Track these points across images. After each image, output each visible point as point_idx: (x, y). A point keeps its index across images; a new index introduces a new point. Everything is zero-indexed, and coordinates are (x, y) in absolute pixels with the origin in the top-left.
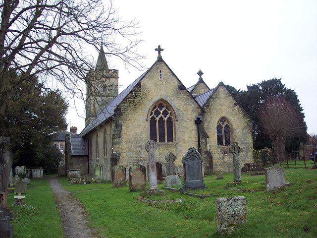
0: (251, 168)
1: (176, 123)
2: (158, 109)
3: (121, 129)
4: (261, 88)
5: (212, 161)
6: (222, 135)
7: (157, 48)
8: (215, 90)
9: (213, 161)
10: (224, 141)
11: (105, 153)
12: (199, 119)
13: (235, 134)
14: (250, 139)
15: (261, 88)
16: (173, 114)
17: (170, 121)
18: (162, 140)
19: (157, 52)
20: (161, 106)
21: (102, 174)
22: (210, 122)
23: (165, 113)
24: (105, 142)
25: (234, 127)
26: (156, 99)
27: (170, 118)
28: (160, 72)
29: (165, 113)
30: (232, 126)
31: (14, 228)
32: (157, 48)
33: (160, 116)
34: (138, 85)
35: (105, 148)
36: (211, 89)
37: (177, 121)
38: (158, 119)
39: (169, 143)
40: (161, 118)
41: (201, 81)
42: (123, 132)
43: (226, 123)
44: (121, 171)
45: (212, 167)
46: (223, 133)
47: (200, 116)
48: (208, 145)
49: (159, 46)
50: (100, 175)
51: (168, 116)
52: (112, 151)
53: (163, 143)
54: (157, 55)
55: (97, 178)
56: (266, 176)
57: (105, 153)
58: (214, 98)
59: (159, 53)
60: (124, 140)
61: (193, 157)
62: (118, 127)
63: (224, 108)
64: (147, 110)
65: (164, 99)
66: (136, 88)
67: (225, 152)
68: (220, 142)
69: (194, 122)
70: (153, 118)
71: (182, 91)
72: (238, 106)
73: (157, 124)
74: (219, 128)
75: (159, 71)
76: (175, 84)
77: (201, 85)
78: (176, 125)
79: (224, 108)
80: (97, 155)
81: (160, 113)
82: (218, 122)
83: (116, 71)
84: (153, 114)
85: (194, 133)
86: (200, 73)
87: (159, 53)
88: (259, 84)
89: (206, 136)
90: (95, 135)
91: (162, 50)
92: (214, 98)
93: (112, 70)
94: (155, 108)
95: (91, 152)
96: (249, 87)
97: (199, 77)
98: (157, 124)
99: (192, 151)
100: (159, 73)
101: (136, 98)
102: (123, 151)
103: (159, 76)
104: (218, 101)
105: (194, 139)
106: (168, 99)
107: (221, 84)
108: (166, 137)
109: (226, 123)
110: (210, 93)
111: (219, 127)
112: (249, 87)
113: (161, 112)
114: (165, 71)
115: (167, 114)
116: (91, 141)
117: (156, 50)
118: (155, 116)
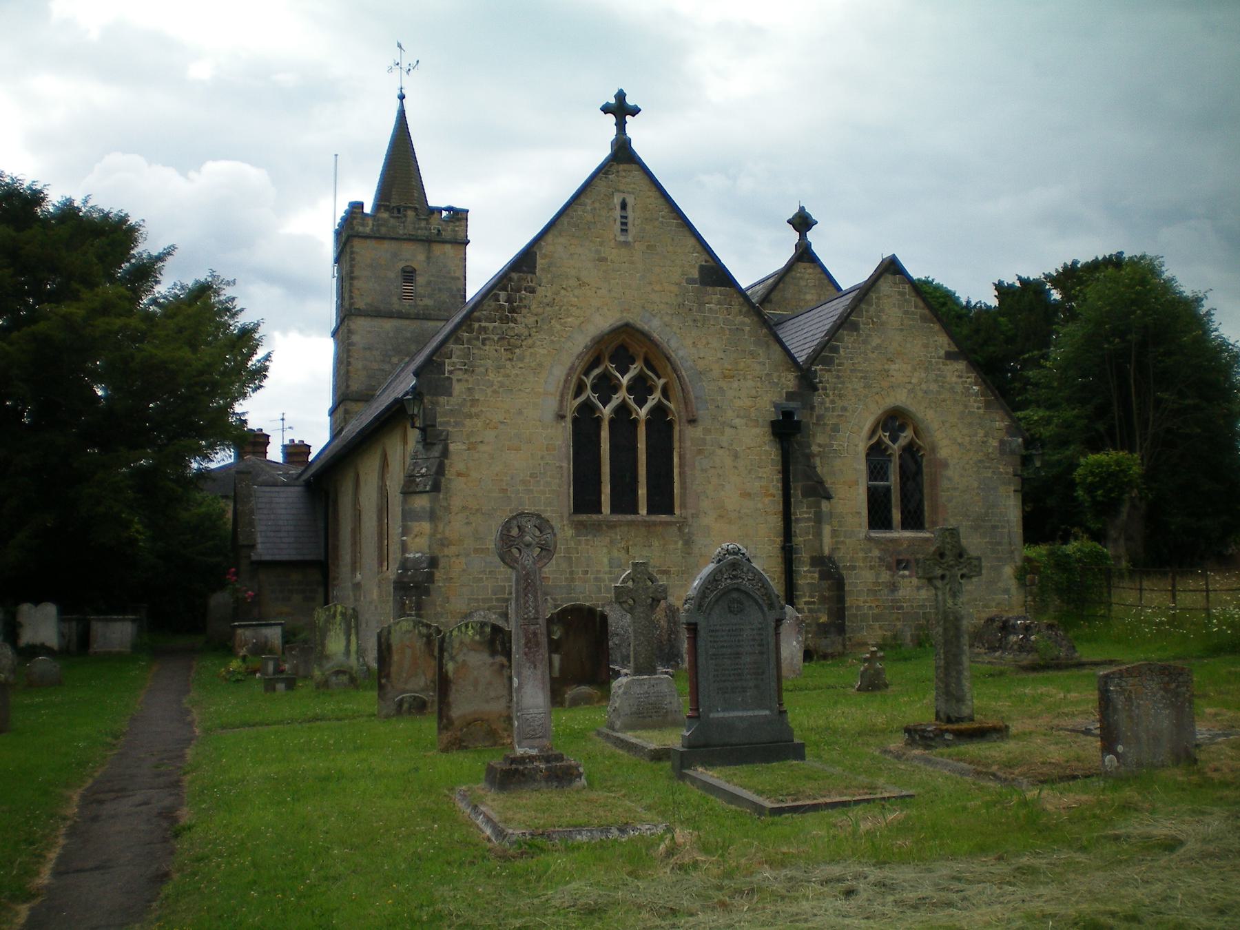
0: (1013, 638)
1: (693, 433)
2: (612, 368)
3: (445, 453)
4: (1056, 295)
5: (841, 599)
6: (888, 489)
7: (613, 101)
8: (865, 291)
9: (849, 601)
10: (896, 515)
11: (382, 558)
12: (788, 414)
13: (945, 484)
14: (1011, 510)
15: (1056, 295)
16: (676, 390)
17: (661, 422)
18: (624, 502)
19: (611, 119)
20: (623, 358)
21: (353, 647)
22: (836, 429)
23: (641, 388)
24: (383, 510)
25: (944, 453)
26: (603, 322)
27: (659, 412)
28: (624, 206)
29: (641, 388)
30: (934, 449)
31: (375, 694)
32: (613, 101)
33: (616, 400)
34: (525, 261)
35: (382, 534)
36: (845, 285)
37: (692, 421)
38: (607, 411)
39: (654, 518)
40: (623, 409)
41: (804, 254)
42: (456, 463)
43: (906, 436)
44: (420, 644)
45: (841, 630)
46: (894, 480)
47: (792, 405)
48: (827, 530)
49: (621, 96)
50: (347, 652)
51: (652, 401)
52: (404, 548)
53: (630, 517)
54: (612, 132)
55: (329, 666)
56: (849, 314)
57: (382, 558)
58: (855, 327)
59: (621, 125)
60: (456, 503)
61: (735, 595)
62: (432, 437)
63: (899, 369)
64: (560, 372)
65: (640, 324)
66: (515, 276)
67: (899, 562)
68: (878, 516)
69: (768, 429)
70: (587, 409)
71: (715, 294)
72: (961, 365)
73: (605, 434)
74: (876, 456)
75: (617, 200)
76: (697, 259)
77: (805, 270)
78: (686, 438)
79: (899, 369)
80: (355, 566)
81: (616, 388)
82: (873, 432)
83: (458, 216)
84: (589, 392)
85: (768, 476)
86: (802, 222)
87: (621, 125)
88: (1047, 276)
89: (819, 491)
90: (350, 476)
91: (635, 111)
92: (855, 327)
93: (440, 210)
94: (595, 363)
95: (336, 548)
96: (1002, 290)
97: (795, 236)
98: (605, 434)
99: (734, 565)
100: (618, 212)
101: (515, 321)
102: (452, 550)
103: (618, 226)
104: (875, 341)
105: (766, 500)
106: (654, 326)
107: (891, 267)
108: (642, 492)
109: (906, 436)
110: (838, 307)
111: (876, 454)
112: (1002, 290)
113: (625, 381)
114: (640, 201)
115: (650, 391)
116: (336, 502)
117: (606, 109)
118: (594, 398)
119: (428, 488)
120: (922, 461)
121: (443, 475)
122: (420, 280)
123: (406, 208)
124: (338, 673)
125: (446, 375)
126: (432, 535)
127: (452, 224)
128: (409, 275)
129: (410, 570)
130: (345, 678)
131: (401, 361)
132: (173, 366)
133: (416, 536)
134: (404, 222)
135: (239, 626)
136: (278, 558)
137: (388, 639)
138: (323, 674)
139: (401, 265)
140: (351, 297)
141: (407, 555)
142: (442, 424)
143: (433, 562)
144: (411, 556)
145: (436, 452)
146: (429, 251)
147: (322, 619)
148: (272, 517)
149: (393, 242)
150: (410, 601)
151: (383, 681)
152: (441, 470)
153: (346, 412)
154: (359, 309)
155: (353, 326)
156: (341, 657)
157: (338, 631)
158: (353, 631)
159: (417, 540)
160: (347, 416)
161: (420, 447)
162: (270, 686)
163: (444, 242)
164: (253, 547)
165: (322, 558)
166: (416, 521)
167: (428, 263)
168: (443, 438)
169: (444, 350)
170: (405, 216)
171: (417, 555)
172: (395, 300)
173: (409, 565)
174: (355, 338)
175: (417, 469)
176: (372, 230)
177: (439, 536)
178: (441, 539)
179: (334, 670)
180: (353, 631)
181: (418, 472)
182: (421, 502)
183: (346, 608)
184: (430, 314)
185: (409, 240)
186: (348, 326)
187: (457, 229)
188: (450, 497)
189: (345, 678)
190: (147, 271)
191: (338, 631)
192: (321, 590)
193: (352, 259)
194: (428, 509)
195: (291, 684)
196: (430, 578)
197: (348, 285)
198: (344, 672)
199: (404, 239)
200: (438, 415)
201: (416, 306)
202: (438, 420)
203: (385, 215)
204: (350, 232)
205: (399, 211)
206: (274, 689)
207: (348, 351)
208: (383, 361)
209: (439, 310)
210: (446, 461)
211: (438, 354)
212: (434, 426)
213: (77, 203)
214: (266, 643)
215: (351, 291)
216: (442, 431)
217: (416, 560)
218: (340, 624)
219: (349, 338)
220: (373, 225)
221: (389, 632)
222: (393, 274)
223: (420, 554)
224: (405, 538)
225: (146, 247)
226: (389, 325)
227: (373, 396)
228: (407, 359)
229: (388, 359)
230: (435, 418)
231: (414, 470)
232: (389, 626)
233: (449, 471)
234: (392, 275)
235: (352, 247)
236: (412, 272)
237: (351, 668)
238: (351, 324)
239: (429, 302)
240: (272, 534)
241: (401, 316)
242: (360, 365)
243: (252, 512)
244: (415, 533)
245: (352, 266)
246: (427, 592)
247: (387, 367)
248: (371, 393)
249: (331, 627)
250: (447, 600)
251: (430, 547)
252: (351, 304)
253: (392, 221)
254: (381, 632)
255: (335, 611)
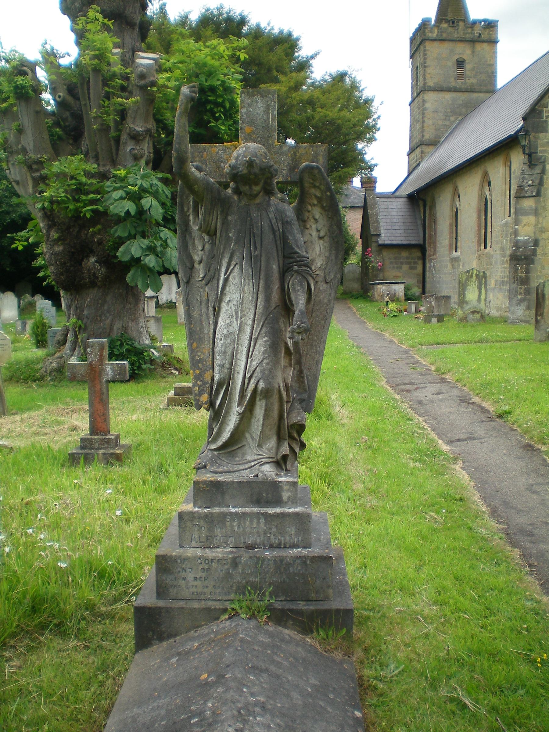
3: (543, 172)
21: (483, 296)
119: (534, 194)
120: (169, 229)
121: (543, 185)
122: (468, 66)
123: (458, 21)
124: (473, 312)
125: (544, 119)
126: (536, 225)
127: (488, 30)
128: (460, 64)
129: (521, 247)
130: (478, 316)
131: (456, 119)
132: (339, 122)
133: (525, 225)
134: (457, 30)
135: (378, 284)
136: (395, 242)
137: (543, 291)
138: (464, 313)
139: (456, 57)
140: (425, 79)
141: (519, 238)
142: (541, 152)
143: (536, 243)
144: (522, 238)
145: (538, 170)
146: (473, 47)
147: (464, 279)
148: (389, 217)
149: (451, 43)
150: (522, 268)
151: (539, 318)
152: (541, 183)
153: (422, 152)
154: (430, 86)
155: (426, 97)
156: (475, 303)
157: (474, 286)
158: (483, 286)
159: (525, 228)
160: (423, 155)
161: (526, 167)
162: (427, 320)
163: (483, 42)
164: (379, 235)
165: (422, 243)
166: (525, 216)
167: (473, 56)
168: (542, 160)
169: (543, 102)
170: (458, 25)
171: (526, 238)
172: (452, 80)
173: (520, 244)
174: (427, 105)
175: (525, 182)
176: (437, 35)
177: (540, 226)
178: (541, 228)
179: (472, 310)
180: (483, 286)
181: (526, 183)
182: (528, 203)
183: (479, 272)
184: (475, 89)
185: (461, 41)
186: (423, 97)
187: (491, 33)
188: (546, 200)
189: (478, 316)
190: (304, 66)
191: (474, 286)
192: (420, 262)
193: (425, 55)
194: (534, 208)
195: (440, 319)
196: (534, 251)
197: (422, 72)
198: (478, 312)
199: (458, 41)
200: (539, 145)
201: (465, 84)
202: (539, 149)
203: (444, 25)
204: (424, 37)
205: (453, 23)
206: (430, 321)
207: (423, 114)
208: (445, 119)
209: (481, 86)
210: (544, 176)
211: (539, 105)
212: (537, 153)
213: (263, 26)
214: (395, 294)
215: (424, 75)
216: (542, 156)
217: (525, 242)
218: (475, 282)
219: (423, 105)
220: (438, 32)
221: (544, 286)
222: (451, 63)
223: (528, 237)
224: (516, 227)
225: (303, 53)
226: (448, 96)
227: (439, 142)
228: (460, 118)
229: (448, 118)
230: (537, 147)
231: (523, 182)
232: (544, 282)
233: (546, 182)
234: (450, 64)
235: (425, 47)
236: (463, 62)
237: (482, 310)
238: (425, 95)
239: (473, 81)
240: (390, 228)
241: (456, 90)
242: (431, 122)
243: (377, 215)
244: (525, 223)
245: (425, 59)
246: (533, 262)
247: (447, 123)
248: (437, 140)
249: (469, 283)
250: (543, 268)
251: (535, 233)
252: (425, 84)
253: (450, 29)
254: (539, 285)
255: (472, 274)
